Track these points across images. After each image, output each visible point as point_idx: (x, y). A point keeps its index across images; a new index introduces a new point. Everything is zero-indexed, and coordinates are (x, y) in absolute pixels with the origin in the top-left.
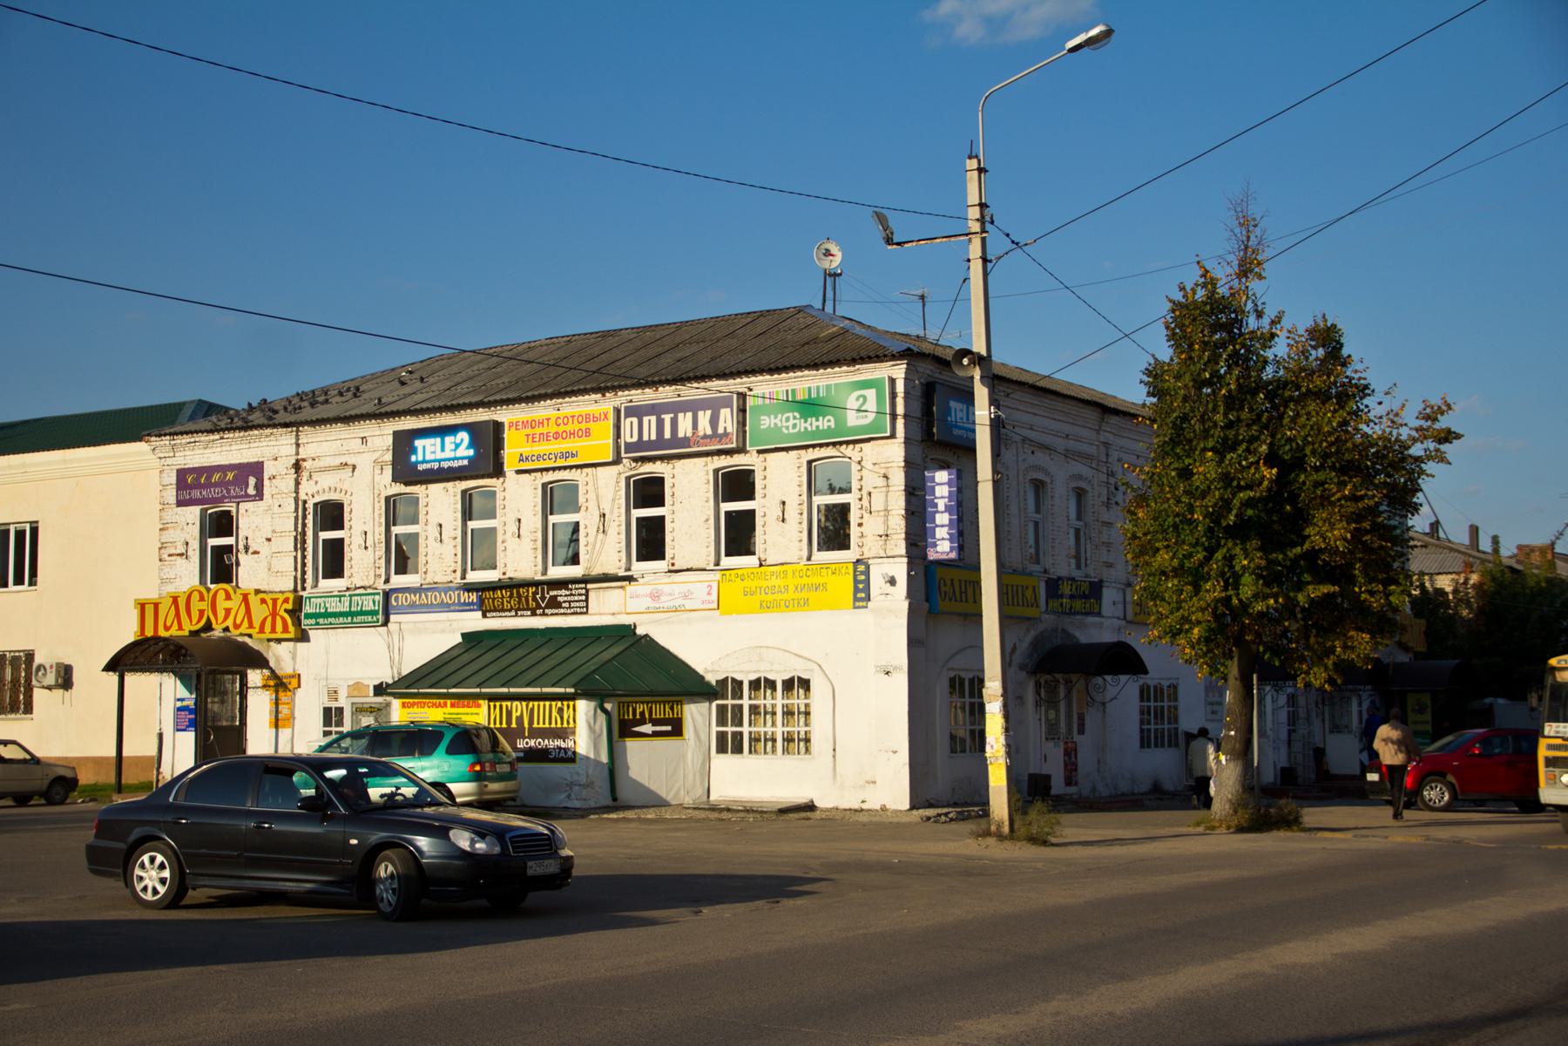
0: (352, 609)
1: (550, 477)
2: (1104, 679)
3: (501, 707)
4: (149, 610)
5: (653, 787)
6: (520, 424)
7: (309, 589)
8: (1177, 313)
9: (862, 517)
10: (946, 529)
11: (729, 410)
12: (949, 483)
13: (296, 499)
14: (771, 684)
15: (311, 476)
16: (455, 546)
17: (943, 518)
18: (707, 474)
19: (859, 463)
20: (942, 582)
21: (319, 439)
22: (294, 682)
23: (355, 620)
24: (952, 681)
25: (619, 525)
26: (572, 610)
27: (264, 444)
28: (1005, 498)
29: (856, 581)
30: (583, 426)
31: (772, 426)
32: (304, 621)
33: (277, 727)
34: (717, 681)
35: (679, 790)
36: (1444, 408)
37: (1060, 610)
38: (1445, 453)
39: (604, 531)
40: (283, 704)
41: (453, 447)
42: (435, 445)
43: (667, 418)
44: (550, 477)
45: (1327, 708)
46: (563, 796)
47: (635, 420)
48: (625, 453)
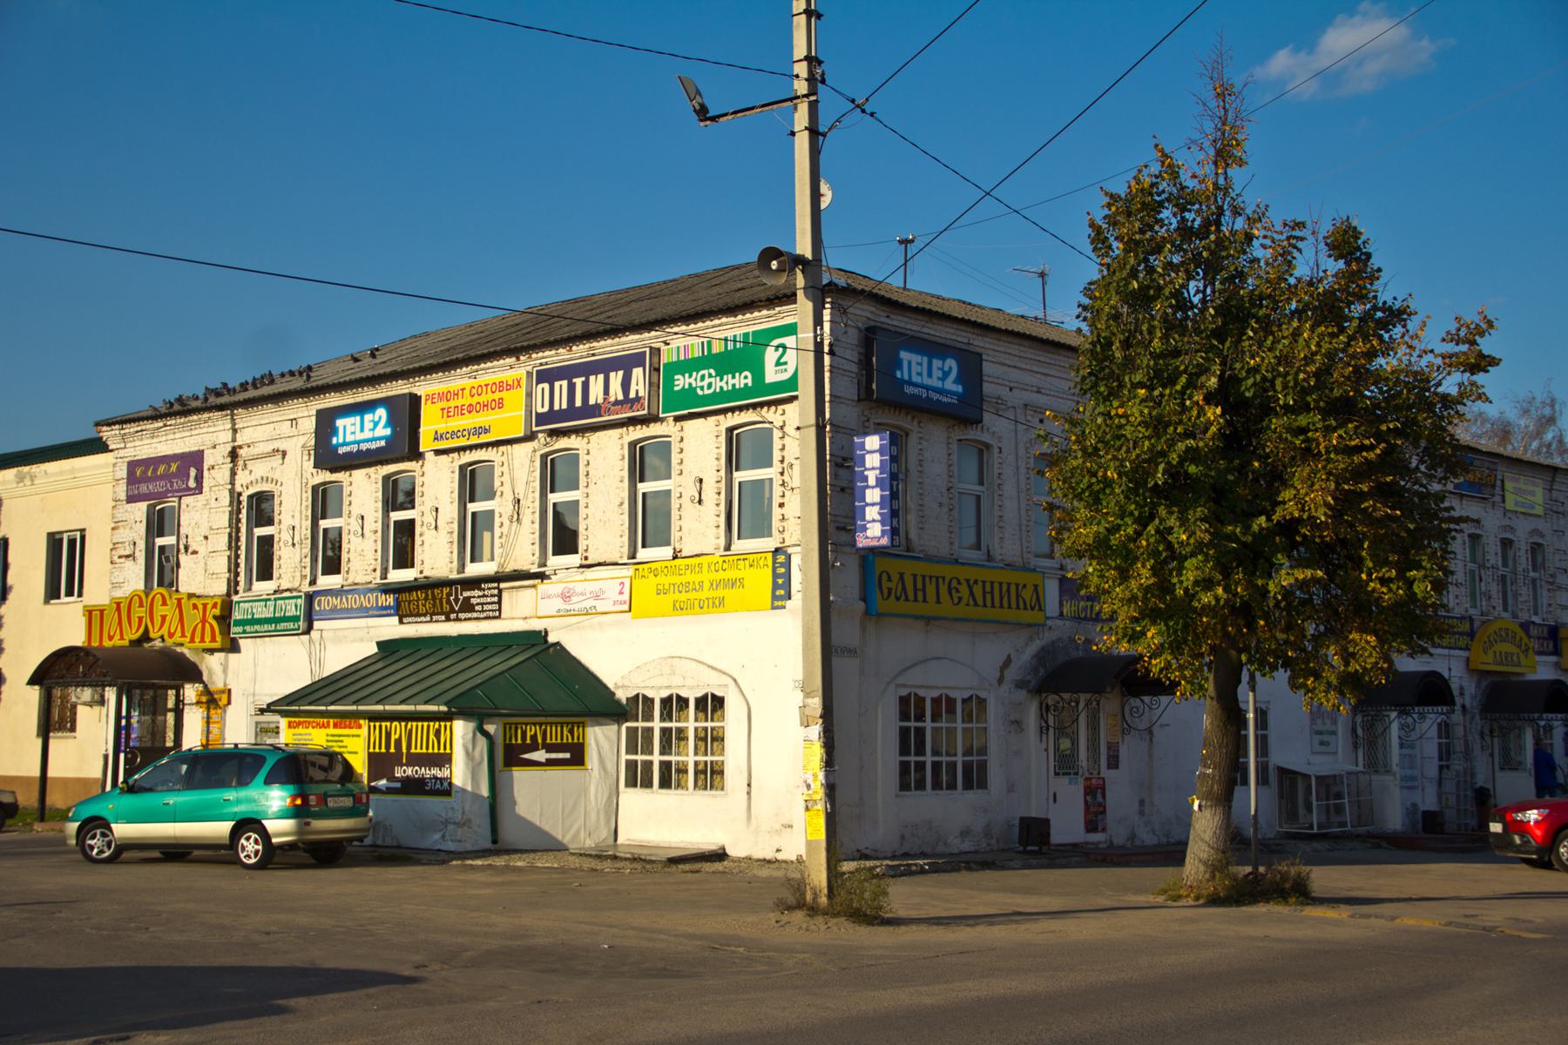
1: (468, 457)
2: (1142, 701)
3: (381, 726)
4: (96, 614)
5: (546, 827)
7: (241, 594)
8: (1113, 209)
9: (783, 496)
11: (641, 369)
12: (881, 451)
13: (232, 491)
14: (683, 702)
15: (245, 465)
16: (376, 541)
17: (873, 495)
18: (622, 448)
19: (782, 428)
20: (885, 577)
21: (254, 423)
22: (224, 700)
24: (904, 701)
25: (534, 513)
26: (485, 614)
27: (205, 430)
28: (996, 475)
29: (775, 576)
30: (497, 396)
31: (687, 387)
32: (234, 629)
34: (628, 699)
35: (578, 832)
36: (1484, 326)
37: (1082, 616)
38: (1483, 387)
39: (518, 519)
40: (215, 722)
41: (371, 425)
42: (354, 424)
43: (578, 381)
44: (468, 457)
45: (1496, 740)
46: (437, 836)
47: (546, 386)
48: (537, 426)
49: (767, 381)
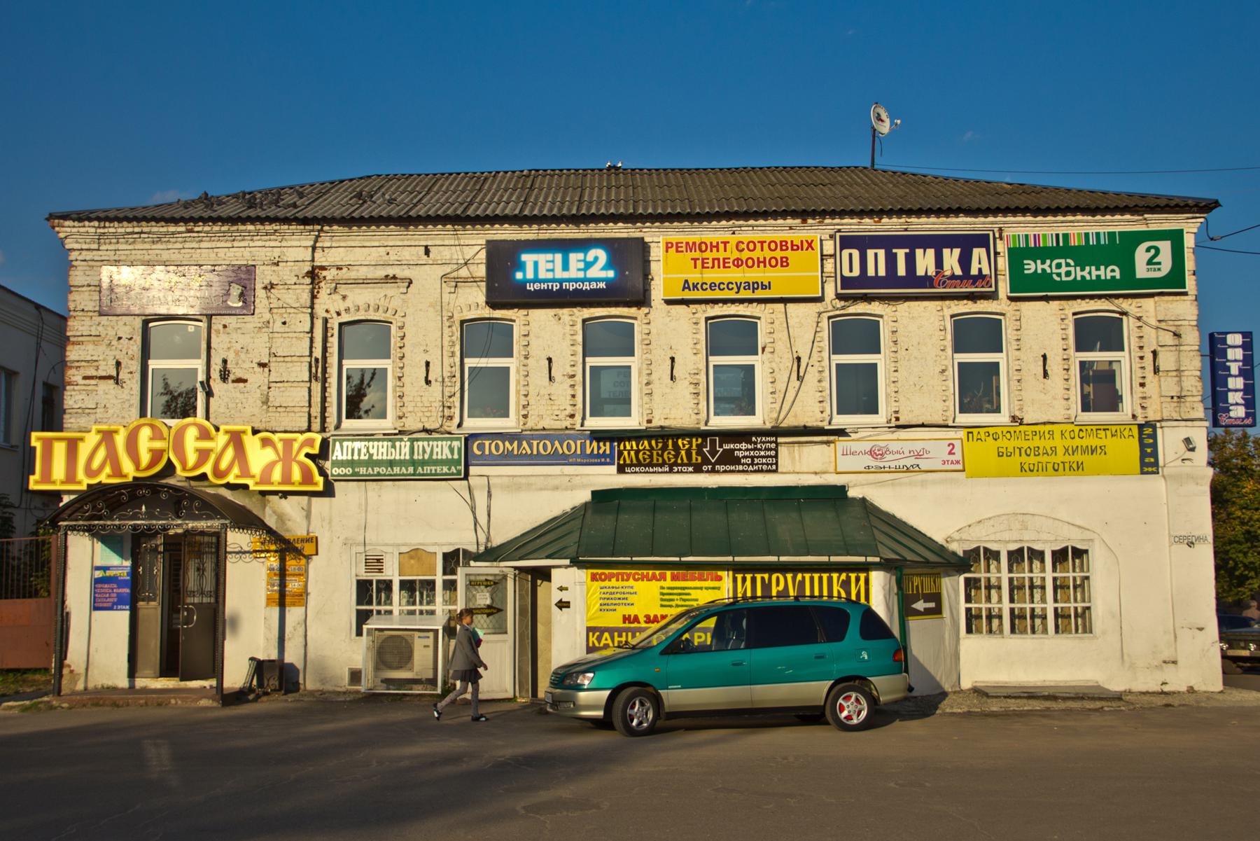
0: (416, 457)
6: (684, 245)
10: (1241, 393)
11: (984, 250)
14: (1038, 555)
15: (336, 288)
16: (573, 386)
23: (420, 470)
30: (778, 254)
33: (282, 604)
41: (582, 265)
49: (1138, 276)
